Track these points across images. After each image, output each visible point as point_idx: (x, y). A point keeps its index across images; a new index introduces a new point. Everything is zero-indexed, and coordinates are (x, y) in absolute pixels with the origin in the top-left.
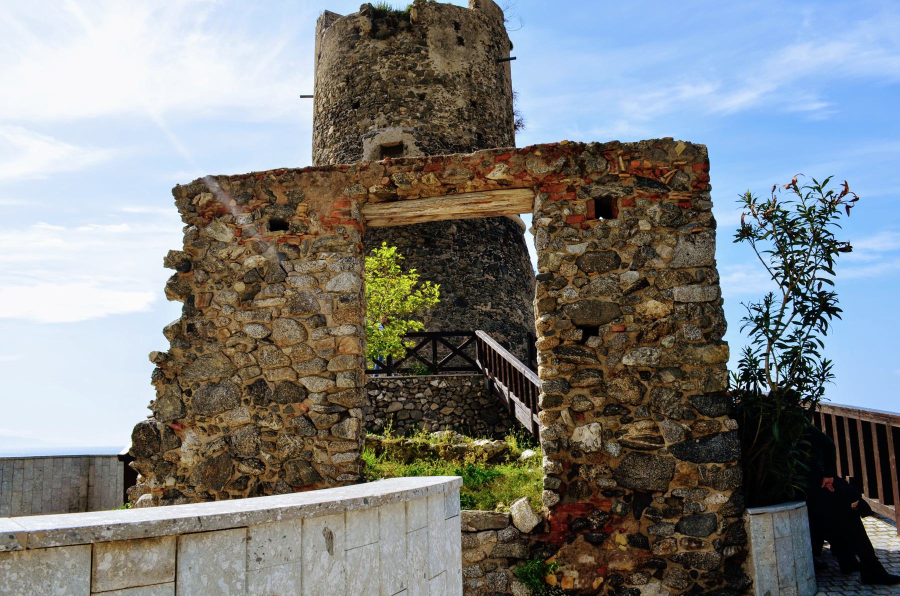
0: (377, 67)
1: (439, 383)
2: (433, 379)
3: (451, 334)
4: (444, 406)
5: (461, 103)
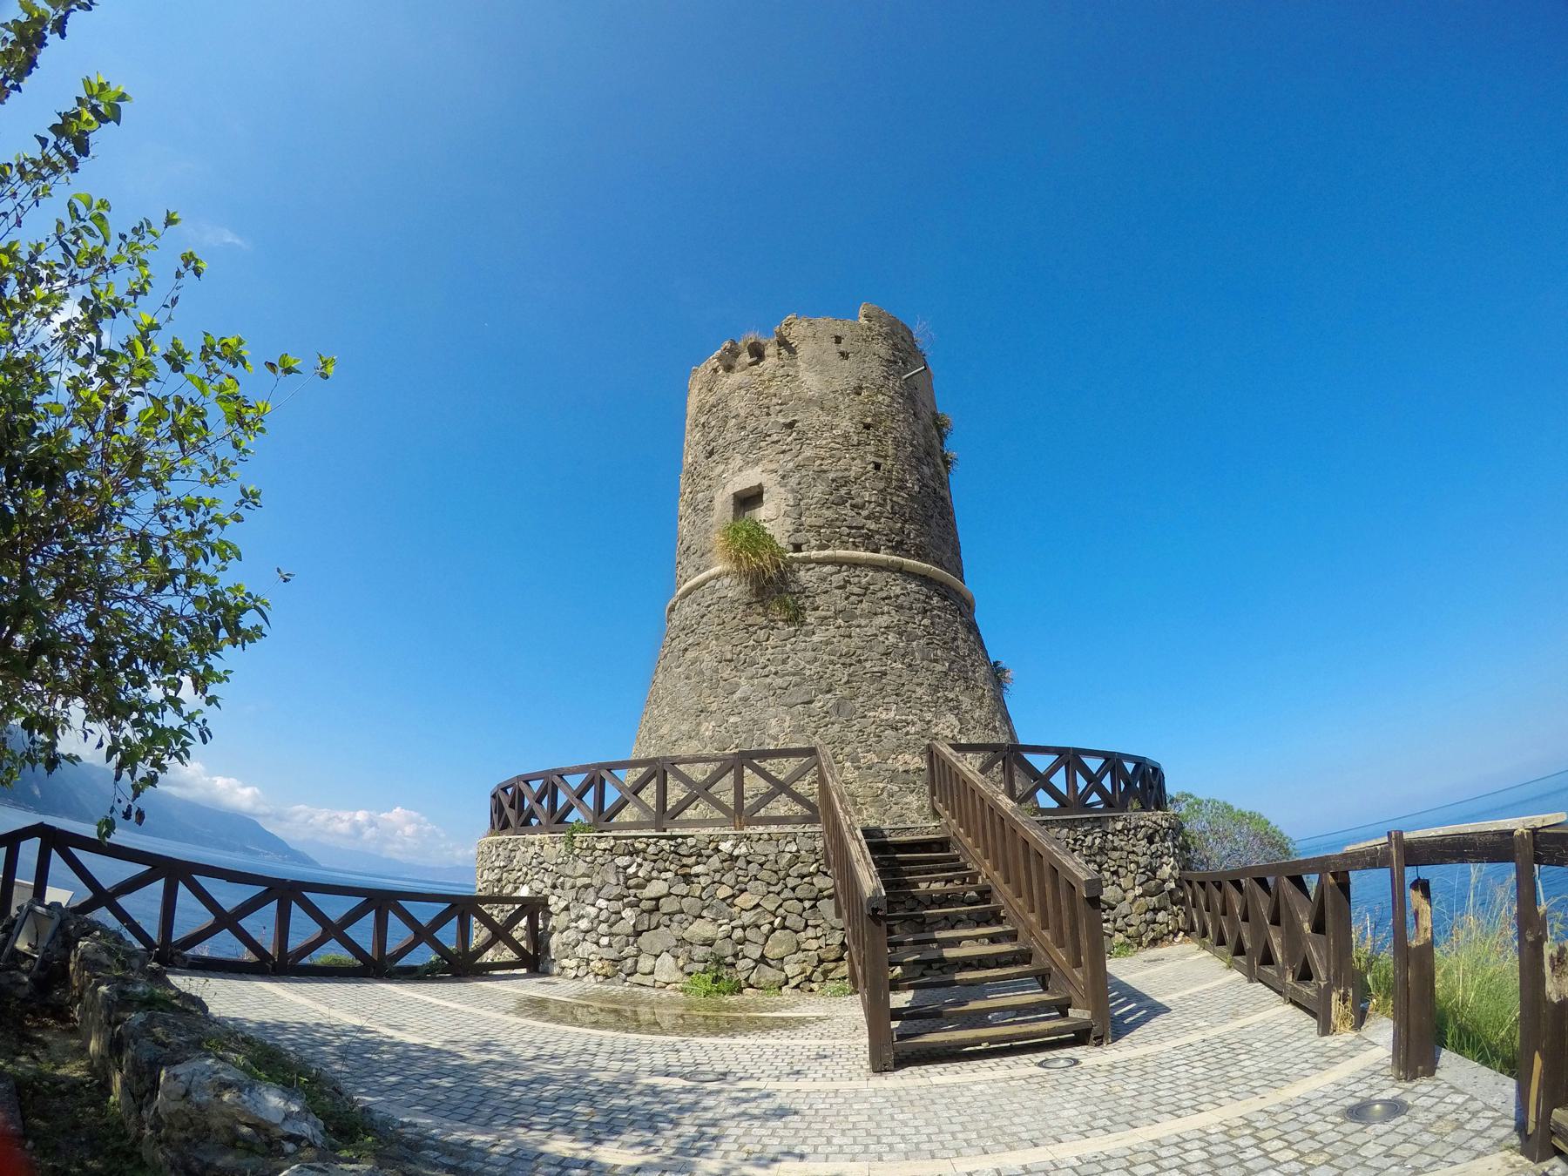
1: (735, 846)
2: (725, 838)
3: (684, 761)
4: (743, 891)
5: (845, 425)
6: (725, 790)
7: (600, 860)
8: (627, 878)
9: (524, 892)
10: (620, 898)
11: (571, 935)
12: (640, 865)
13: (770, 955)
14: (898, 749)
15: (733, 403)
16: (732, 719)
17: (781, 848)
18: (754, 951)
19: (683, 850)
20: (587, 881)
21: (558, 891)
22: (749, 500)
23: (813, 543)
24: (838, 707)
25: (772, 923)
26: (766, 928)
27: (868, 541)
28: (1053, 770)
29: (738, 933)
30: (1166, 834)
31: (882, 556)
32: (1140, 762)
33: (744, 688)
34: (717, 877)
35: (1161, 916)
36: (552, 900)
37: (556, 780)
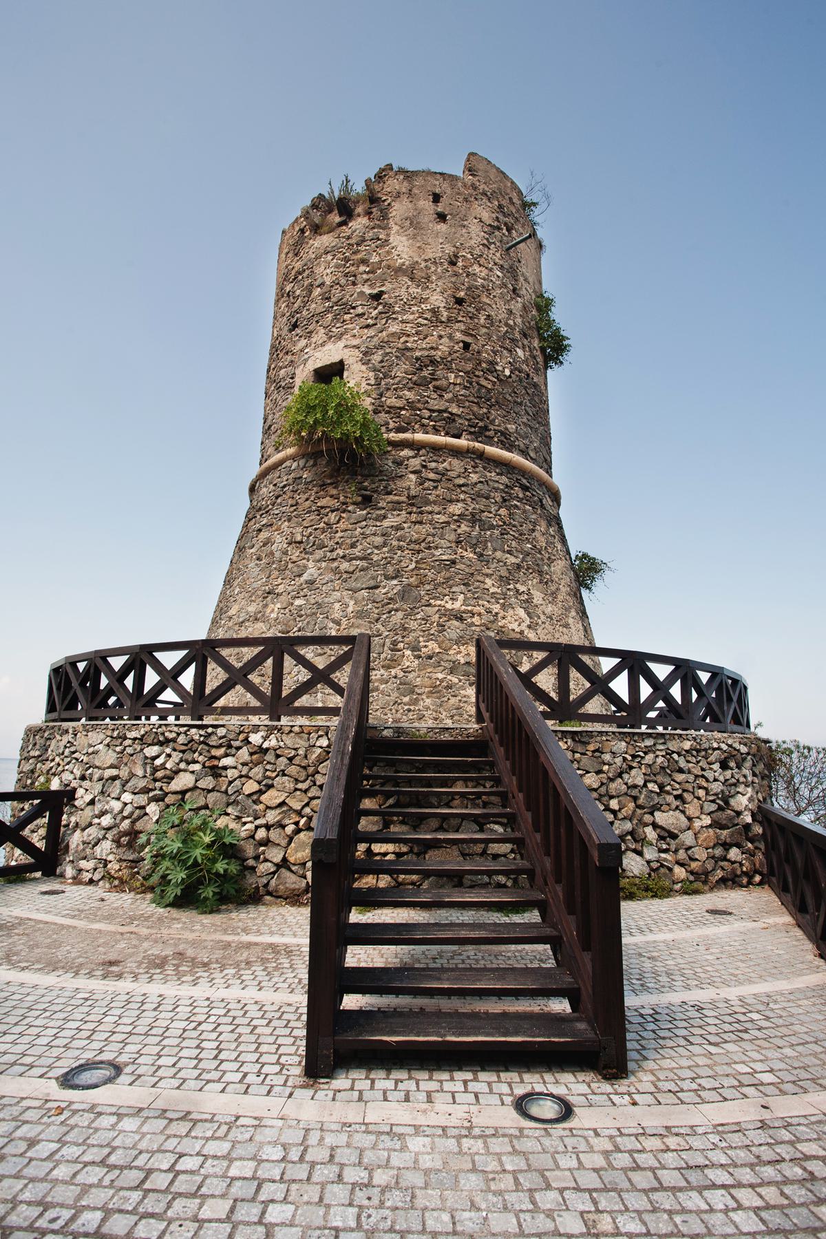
1: (265, 738)
2: (256, 729)
5: (437, 300)
6: (261, 678)
7: (129, 750)
8: (155, 770)
9: (55, 785)
10: (145, 791)
11: (93, 832)
12: (169, 756)
13: (292, 859)
14: (460, 641)
15: (319, 270)
16: (298, 602)
17: (312, 742)
18: (276, 855)
19: (213, 741)
20: (114, 772)
21: (86, 784)
22: (330, 374)
23: (392, 425)
24: (404, 594)
25: (297, 823)
26: (290, 829)
27: (448, 423)
28: (614, 673)
29: (261, 834)
30: (744, 760)
31: (463, 442)
32: (716, 672)
33: (311, 572)
34: (245, 770)
35: (734, 854)
36: (80, 792)
37: (99, 663)
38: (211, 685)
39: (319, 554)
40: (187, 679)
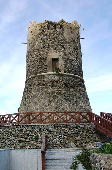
0: (51, 37)
2: (80, 125)
5: (73, 49)
7: (59, 128)
10: (64, 134)
16: (58, 103)
29: (83, 139)
31: (77, 76)
37: (4, 116)
38: (20, 119)
39: (60, 95)
40: (17, 119)
